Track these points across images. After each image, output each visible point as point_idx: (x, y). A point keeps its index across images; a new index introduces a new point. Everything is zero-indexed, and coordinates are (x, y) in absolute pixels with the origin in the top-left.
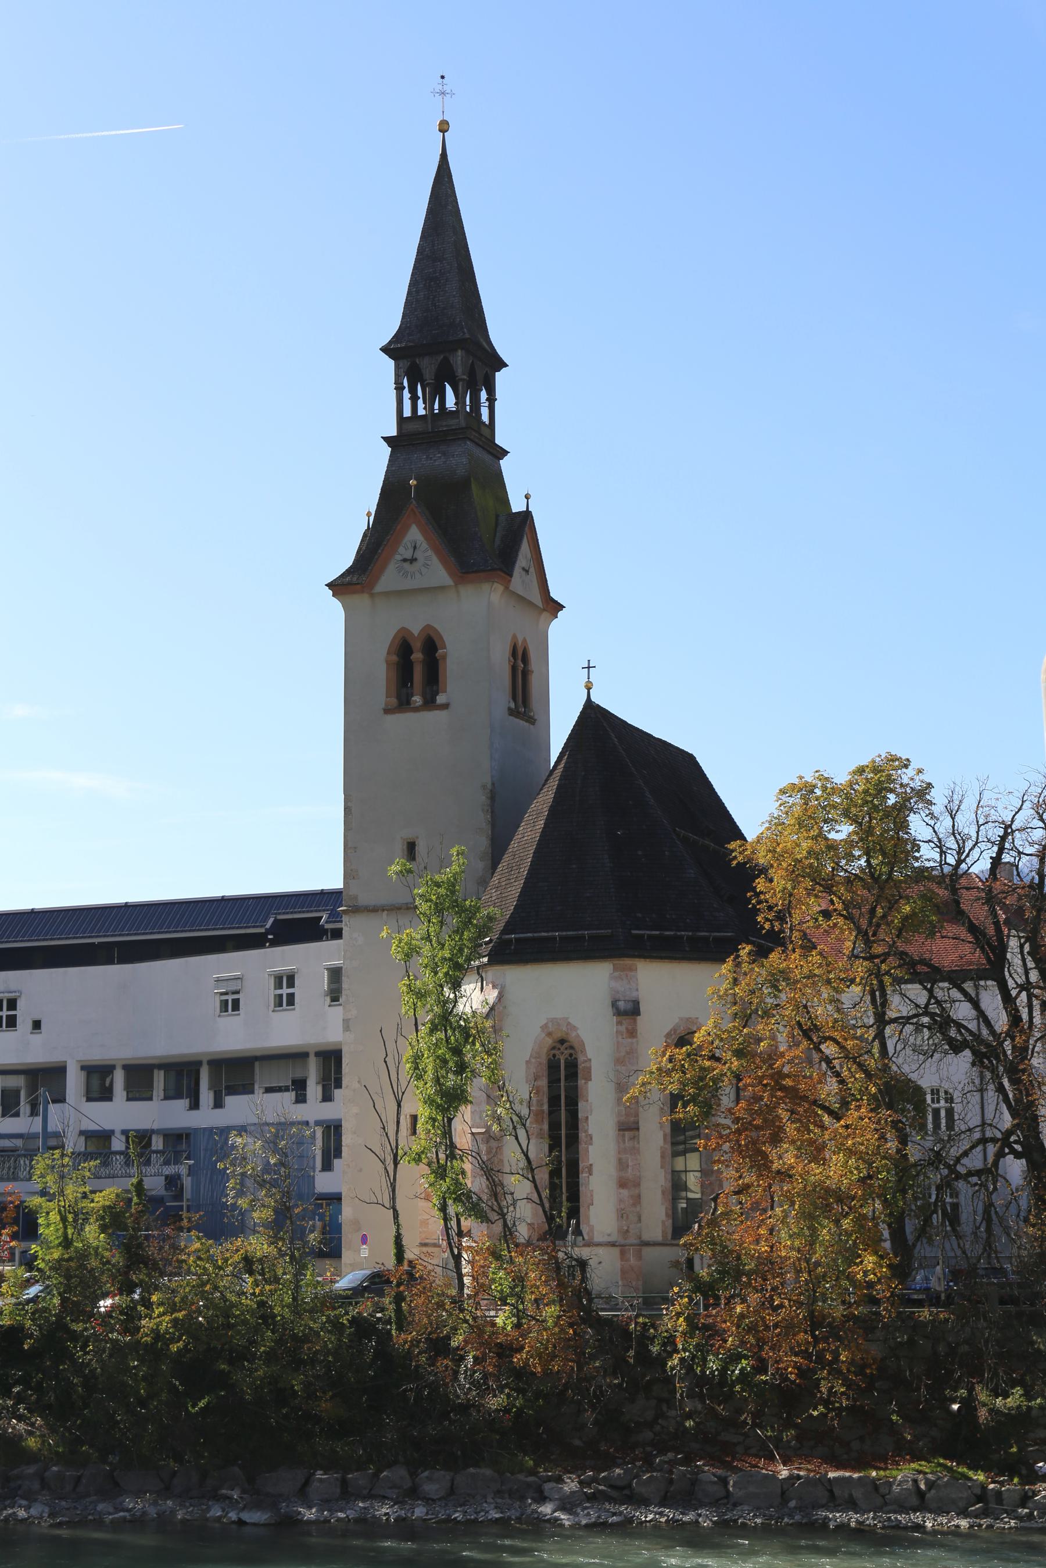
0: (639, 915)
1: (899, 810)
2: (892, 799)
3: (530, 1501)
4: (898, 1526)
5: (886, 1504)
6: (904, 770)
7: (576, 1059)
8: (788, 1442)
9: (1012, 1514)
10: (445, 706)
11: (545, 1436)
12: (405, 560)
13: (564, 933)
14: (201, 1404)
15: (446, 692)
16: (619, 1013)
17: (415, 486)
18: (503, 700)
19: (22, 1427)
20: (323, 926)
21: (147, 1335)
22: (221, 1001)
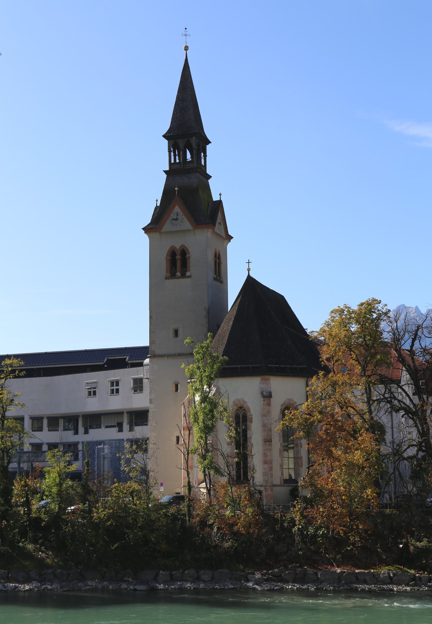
0: (271, 359)
1: (378, 320)
2: (375, 316)
3: (243, 581)
4: (384, 590)
5: (378, 582)
6: (379, 304)
7: (246, 414)
8: (339, 559)
9: (426, 585)
10: (190, 277)
11: (245, 558)
12: (173, 219)
13: (242, 366)
14: (115, 546)
15: (190, 271)
16: (264, 396)
17: (177, 190)
18: (212, 274)
19: (44, 555)
20: (127, 362)
21: (96, 519)
22: (88, 391)
